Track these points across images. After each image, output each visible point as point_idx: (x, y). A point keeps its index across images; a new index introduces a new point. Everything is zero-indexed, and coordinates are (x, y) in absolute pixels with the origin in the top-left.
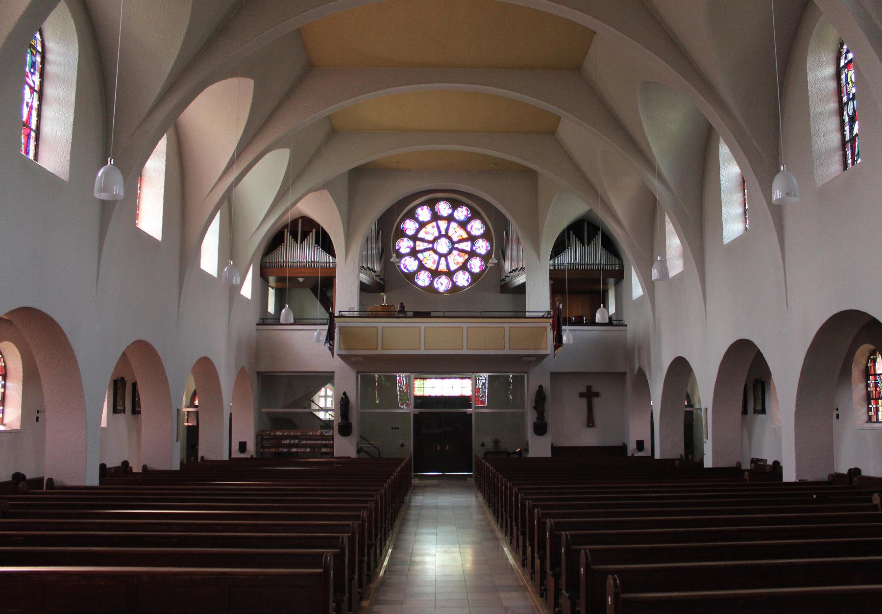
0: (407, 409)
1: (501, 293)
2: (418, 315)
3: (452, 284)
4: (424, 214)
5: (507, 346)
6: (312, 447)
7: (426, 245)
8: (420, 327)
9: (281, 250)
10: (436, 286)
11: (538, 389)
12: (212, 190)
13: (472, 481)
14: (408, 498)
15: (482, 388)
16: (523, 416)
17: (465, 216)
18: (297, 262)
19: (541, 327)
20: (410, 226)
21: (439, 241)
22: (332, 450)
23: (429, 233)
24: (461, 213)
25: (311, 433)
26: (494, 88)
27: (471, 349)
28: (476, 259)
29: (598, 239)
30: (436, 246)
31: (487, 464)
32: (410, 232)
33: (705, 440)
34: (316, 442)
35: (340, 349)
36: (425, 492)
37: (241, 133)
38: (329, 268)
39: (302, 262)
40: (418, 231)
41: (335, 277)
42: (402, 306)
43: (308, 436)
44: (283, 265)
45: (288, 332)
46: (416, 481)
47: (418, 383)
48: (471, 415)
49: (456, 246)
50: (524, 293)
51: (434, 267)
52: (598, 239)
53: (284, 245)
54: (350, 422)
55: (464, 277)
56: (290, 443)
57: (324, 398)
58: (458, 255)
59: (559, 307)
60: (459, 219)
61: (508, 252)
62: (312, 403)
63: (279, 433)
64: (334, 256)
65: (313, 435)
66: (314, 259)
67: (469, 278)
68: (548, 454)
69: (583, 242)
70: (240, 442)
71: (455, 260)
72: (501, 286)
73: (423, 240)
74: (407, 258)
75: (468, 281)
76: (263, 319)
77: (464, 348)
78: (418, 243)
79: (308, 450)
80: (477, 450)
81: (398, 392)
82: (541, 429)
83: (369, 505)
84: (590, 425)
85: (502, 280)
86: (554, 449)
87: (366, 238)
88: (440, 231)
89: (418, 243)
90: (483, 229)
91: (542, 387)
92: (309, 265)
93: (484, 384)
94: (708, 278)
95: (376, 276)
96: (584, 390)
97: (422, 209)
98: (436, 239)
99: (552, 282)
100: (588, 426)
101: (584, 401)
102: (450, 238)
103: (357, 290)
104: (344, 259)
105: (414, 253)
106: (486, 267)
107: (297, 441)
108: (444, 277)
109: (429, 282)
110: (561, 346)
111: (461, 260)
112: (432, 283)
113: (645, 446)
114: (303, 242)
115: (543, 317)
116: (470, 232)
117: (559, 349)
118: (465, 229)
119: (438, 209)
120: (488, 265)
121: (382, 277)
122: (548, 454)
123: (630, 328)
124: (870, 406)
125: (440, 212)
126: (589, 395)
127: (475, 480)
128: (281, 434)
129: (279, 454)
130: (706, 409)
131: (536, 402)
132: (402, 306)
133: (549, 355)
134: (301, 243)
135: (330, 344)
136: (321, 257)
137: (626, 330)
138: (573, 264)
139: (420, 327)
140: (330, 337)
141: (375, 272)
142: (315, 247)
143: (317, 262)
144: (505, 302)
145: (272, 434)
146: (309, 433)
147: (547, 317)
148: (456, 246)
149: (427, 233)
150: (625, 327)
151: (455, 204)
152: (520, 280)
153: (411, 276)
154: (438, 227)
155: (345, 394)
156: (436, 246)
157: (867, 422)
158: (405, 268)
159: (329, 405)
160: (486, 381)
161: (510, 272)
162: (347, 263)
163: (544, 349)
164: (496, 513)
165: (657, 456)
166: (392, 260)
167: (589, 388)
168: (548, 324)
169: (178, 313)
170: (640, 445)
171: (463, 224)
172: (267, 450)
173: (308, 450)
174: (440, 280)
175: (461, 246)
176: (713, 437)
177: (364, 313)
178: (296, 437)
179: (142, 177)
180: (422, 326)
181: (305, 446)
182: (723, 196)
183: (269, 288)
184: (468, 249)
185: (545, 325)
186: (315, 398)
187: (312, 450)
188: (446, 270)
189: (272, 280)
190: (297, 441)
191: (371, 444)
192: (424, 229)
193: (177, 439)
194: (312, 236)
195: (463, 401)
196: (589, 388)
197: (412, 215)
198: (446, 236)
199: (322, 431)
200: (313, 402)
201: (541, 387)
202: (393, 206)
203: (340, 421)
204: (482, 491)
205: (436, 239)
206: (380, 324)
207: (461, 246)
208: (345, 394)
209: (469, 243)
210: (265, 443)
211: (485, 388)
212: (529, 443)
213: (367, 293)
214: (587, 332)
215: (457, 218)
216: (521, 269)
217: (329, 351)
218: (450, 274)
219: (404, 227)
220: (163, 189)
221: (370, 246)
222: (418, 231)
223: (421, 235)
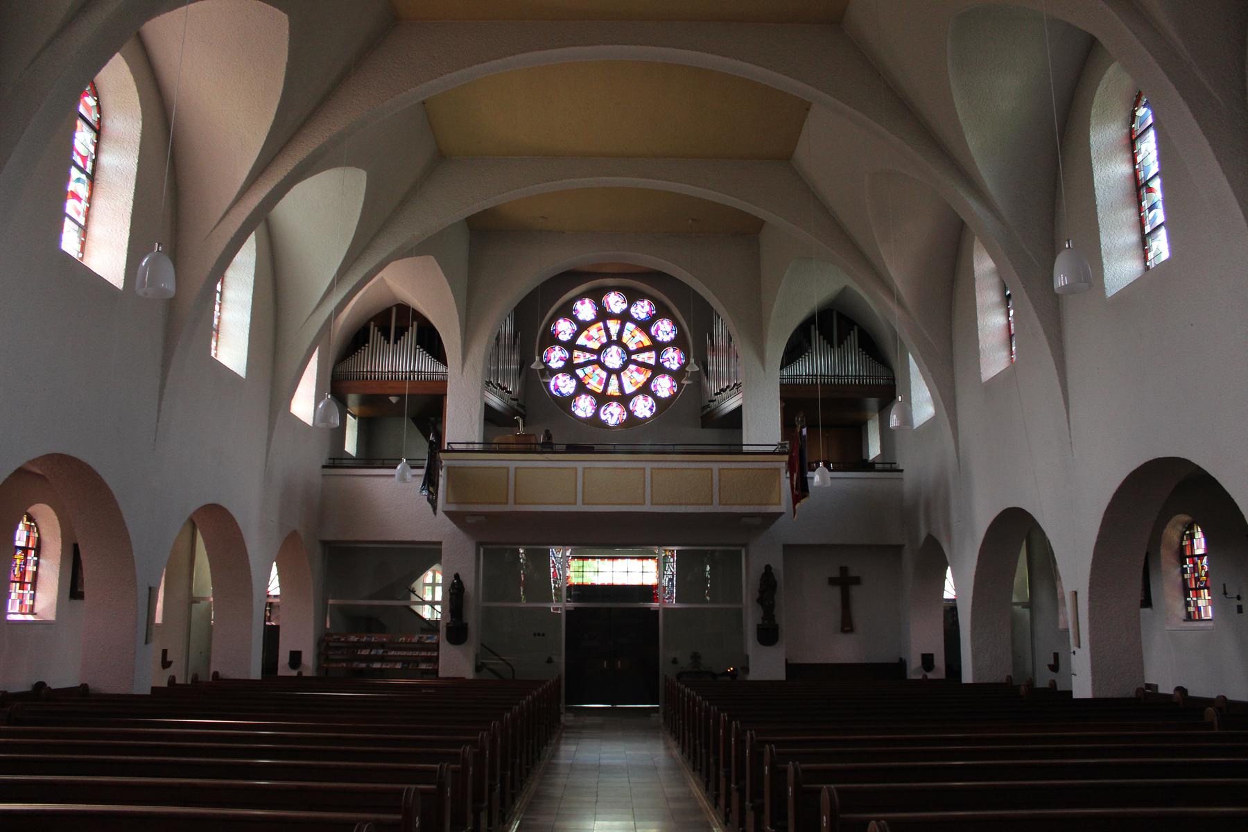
0: (559, 606)
1: (703, 427)
2: (573, 449)
3: (627, 415)
4: (585, 310)
5: (716, 498)
6: (405, 660)
7: (588, 356)
8: (576, 469)
9: (365, 353)
10: (603, 417)
11: (763, 571)
12: (224, 217)
13: (658, 719)
14: (550, 749)
15: (668, 586)
16: (739, 614)
17: (648, 313)
18: (389, 371)
19: (771, 469)
20: (564, 329)
21: (608, 350)
22: (436, 667)
23: (594, 337)
24: (642, 310)
25: (404, 639)
26: (698, 53)
27: (657, 504)
28: (664, 377)
29: (853, 338)
30: (604, 357)
31: (687, 690)
32: (564, 337)
33: (1073, 648)
34: (410, 653)
35: (447, 502)
36: (580, 738)
37: (271, 118)
38: (437, 381)
39: (396, 372)
40: (576, 335)
41: (446, 395)
42: (548, 435)
43: (398, 643)
44: (367, 377)
45: (371, 479)
46: (567, 718)
47: (575, 564)
48: (656, 612)
49: (634, 357)
50: (741, 427)
51: (599, 389)
52: (853, 338)
53: (368, 347)
54: (465, 621)
55: (646, 404)
56: (369, 655)
57: (430, 588)
58: (637, 370)
59: (801, 432)
60: (639, 317)
61: (712, 368)
62: (412, 595)
63: (353, 638)
64: (445, 363)
65: (406, 643)
66: (418, 368)
67: (653, 406)
68: (781, 675)
69: (830, 343)
70: (291, 652)
71: (633, 379)
72: (702, 418)
73: (584, 349)
74: (560, 375)
75: (651, 409)
76: (334, 459)
77: (647, 502)
78: (576, 353)
79: (399, 666)
80: (666, 670)
81: (553, 591)
82: (768, 635)
83: (438, 766)
84: (846, 629)
85: (704, 408)
86: (791, 668)
87: (496, 335)
88: (608, 335)
89: (576, 353)
90: (674, 332)
91: (771, 568)
92: (406, 376)
93: (671, 580)
94: (1070, 362)
95: (511, 399)
96: (836, 573)
97: (583, 303)
98: (604, 347)
99: (784, 404)
100: (843, 631)
101: (836, 591)
102: (624, 347)
103: (480, 415)
104: (460, 366)
105: (570, 368)
106: (679, 389)
107: (381, 652)
108: (615, 404)
109: (593, 411)
110: (805, 496)
111: (641, 378)
112: (597, 414)
113: (936, 663)
114: (399, 342)
115: (773, 453)
116: (655, 337)
117: (803, 501)
118: (648, 333)
119: (608, 303)
120: (683, 382)
121: (520, 402)
122: (781, 675)
123: (906, 475)
124: (1188, 599)
125: (609, 308)
126: (845, 582)
127: (665, 718)
128: (356, 639)
129: (360, 673)
130: (1076, 593)
131: (762, 592)
132: (548, 435)
133: (783, 513)
134: (395, 342)
135: (430, 492)
136: (425, 365)
137: (902, 479)
138: (824, 376)
139: (576, 469)
140: (430, 481)
141: (510, 392)
142: (416, 349)
143: (418, 372)
144: (710, 436)
145: (343, 639)
146: (400, 639)
147: (780, 453)
148: (634, 357)
149: (590, 338)
150: (901, 473)
151: (632, 297)
152: (731, 404)
153: (566, 403)
154: (607, 330)
155: (457, 576)
156: (604, 357)
157: (1184, 620)
158: (556, 390)
159: (439, 597)
160: (673, 577)
161: (717, 394)
162: (464, 374)
163: (775, 504)
164: (710, 784)
165: (967, 677)
166: (533, 366)
167: (844, 570)
168: (782, 463)
169: (158, 421)
170: (927, 661)
171: (644, 326)
172: (334, 665)
173: (399, 666)
174: (610, 409)
175: (642, 357)
176: (1093, 643)
177: (489, 447)
178: (382, 645)
179: (96, 182)
180: (580, 466)
181: (395, 660)
182: (1100, 215)
183: (348, 415)
184: (652, 362)
185: (777, 465)
186: (417, 585)
187: (405, 665)
188: (618, 394)
189: (353, 400)
190: (381, 652)
191: (502, 659)
192: (585, 333)
193: (146, 640)
194: (411, 334)
195: (646, 592)
196: (844, 570)
197: (567, 312)
198: (620, 343)
199: (420, 636)
200: (414, 592)
201: (768, 568)
202: (536, 289)
203: (448, 620)
204: (679, 738)
205: (604, 347)
206: (513, 462)
207: (642, 357)
208: (457, 576)
209: (653, 354)
210: (330, 653)
211: (673, 584)
212: (750, 659)
213: (499, 426)
214: (844, 480)
215: (636, 316)
216: (734, 386)
217: (428, 503)
218: (624, 399)
219: (555, 330)
220: (131, 203)
221: (501, 358)
222: (576, 335)
223: (581, 341)
